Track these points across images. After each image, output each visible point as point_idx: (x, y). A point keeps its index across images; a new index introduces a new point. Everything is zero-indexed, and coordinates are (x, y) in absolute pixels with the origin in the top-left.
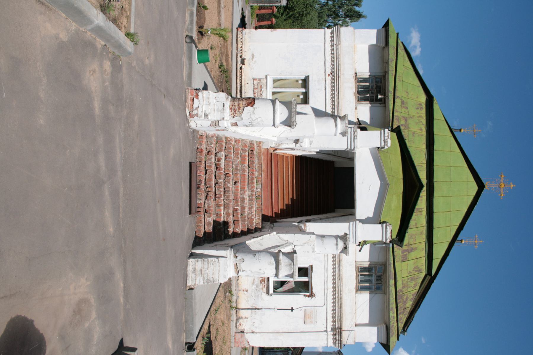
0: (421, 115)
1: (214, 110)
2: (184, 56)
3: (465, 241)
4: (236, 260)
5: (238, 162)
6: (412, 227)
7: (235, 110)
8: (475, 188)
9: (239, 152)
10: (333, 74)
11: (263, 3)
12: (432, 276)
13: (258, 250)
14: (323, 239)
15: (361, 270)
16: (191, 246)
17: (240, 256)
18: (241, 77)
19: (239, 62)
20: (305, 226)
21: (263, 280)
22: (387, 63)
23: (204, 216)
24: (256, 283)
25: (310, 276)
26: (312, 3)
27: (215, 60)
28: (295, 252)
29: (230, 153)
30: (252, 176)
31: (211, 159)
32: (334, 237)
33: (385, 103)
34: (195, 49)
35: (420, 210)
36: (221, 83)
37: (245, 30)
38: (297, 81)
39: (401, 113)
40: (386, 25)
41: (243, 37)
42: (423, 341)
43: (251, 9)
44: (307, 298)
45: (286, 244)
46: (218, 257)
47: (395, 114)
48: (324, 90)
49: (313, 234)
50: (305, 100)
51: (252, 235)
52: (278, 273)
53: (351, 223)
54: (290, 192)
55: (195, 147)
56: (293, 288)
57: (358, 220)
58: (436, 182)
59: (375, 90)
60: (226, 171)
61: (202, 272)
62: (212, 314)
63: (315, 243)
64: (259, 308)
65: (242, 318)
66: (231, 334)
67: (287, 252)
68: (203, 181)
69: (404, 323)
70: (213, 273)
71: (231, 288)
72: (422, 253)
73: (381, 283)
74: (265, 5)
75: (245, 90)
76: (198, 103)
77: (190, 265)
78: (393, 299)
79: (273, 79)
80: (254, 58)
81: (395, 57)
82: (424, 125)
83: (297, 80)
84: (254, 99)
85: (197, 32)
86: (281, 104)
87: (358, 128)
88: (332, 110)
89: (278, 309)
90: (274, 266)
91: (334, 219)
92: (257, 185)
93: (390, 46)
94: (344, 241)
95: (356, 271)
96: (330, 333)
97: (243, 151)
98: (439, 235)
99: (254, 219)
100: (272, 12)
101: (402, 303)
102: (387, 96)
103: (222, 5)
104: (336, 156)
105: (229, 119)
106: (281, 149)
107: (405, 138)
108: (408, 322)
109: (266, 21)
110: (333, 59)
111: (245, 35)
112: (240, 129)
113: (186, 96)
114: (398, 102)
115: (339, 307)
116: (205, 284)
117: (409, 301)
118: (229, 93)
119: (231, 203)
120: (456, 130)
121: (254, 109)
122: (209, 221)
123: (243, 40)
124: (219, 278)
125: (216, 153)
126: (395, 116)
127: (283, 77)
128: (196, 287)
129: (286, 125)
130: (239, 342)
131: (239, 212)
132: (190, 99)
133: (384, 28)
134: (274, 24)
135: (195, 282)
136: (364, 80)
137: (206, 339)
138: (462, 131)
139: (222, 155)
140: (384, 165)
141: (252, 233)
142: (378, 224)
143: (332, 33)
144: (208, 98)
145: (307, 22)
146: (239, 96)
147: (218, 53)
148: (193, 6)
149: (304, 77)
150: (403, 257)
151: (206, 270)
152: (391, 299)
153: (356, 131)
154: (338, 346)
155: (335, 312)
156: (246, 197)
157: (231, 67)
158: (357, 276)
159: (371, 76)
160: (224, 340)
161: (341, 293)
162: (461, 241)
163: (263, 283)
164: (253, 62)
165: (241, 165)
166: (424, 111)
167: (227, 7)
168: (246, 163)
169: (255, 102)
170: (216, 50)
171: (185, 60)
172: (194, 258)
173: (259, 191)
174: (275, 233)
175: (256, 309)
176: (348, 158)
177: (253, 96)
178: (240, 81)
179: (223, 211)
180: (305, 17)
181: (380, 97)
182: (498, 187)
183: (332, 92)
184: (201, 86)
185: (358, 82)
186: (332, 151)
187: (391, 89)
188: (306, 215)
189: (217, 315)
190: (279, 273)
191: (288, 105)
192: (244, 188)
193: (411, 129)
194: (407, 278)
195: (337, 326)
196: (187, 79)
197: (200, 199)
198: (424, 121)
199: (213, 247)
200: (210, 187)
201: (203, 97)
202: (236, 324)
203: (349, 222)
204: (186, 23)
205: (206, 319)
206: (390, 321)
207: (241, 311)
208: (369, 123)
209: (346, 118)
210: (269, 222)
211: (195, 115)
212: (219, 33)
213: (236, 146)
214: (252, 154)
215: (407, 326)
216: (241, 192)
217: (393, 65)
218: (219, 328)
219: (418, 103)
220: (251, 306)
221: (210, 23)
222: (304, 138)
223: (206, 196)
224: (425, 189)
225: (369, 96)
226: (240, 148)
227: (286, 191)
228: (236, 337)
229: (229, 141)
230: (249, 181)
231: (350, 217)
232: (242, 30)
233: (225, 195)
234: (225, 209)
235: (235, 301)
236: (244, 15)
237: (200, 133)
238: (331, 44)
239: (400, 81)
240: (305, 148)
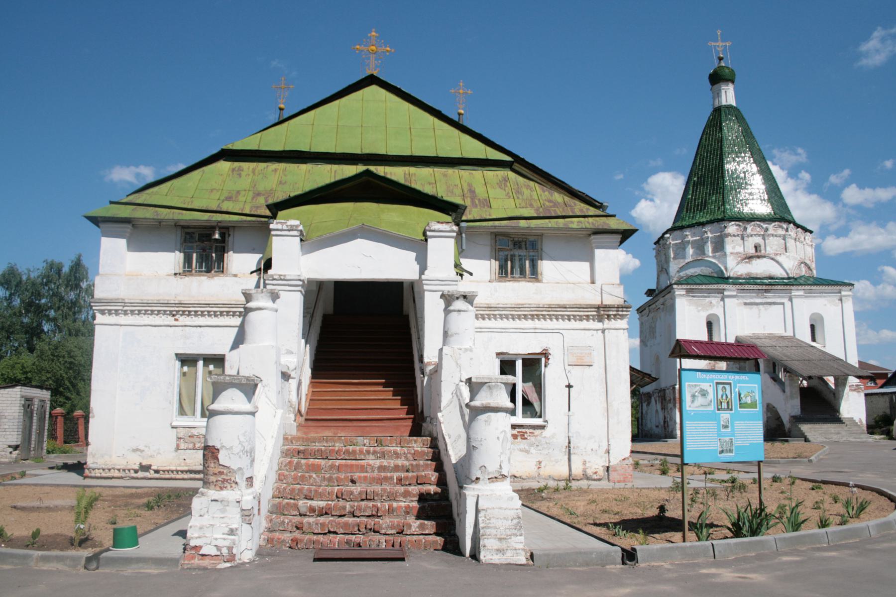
0: (251, 169)
1: (223, 518)
2: (122, 573)
3: (460, 109)
4: (483, 480)
5: (317, 476)
6: (435, 190)
7: (224, 481)
8: (373, 90)
9: (299, 474)
10: (174, 313)
11: (44, 432)
12: (512, 160)
13: (466, 442)
14: (449, 333)
15: (503, 273)
16: (460, 557)
17: (476, 473)
18: (172, 471)
19: (147, 474)
20: (429, 364)
21: (521, 435)
22: (160, 223)
23: (408, 536)
24: (527, 448)
25: (515, 357)
26: (51, 347)
27: (137, 516)
28: (469, 381)
29: (300, 490)
30: (342, 453)
31: (309, 523)
32: (446, 315)
33: (227, 228)
34: (111, 552)
35: (407, 176)
36: (179, 506)
37: (88, 463)
38: (184, 374)
39: (245, 202)
40: (96, 220)
41: (101, 467)
42: (621, 177)
43: (53, 453)
44: (550, 362)
45: (457, 396)
46: (477, 511)
47: (247, 211)
48: (202, 328)
49: (441, 350)
50: (218, 360)
51: (442, 453)
52: (503, 408)
53: (425, 287)
54: (373, 389)
55: (288, 551)
56: (535, 386)
57: (420, 277)
58: (362, 149)
59: (206, 243)
60: (332, 497)
61: (503, 539)
62: (576, 521)
63: (456, 347)
64: (567, 441)
65: (584, 471)
66: (611, 487)
67: (469, 394)
68: (347, 537)
69: (588, 207)
70: (504, 518)
71: (534, 489)
72: (477, 175)
73: (525, 241)
74: (46, 428)
75: (195, 465)
76: (209, 546)
77: (491, 559)
78: (550, 222)
79: (179, 415)
80: (139, 448)
81: (152, 208)
82: (267, 166)
83: (182, 374)
84: (206, 448)
85: (80, 548)
86: (216, 401)
87: (267, 273)
88: (237, 315)
89: (569, 410)
90: (492, 415)
91: (419, 315)
92: (358, 444)
93: (132, 216)
94: (454, 300)
95: (505, 282)
96: (607, 324)
97: (298, 469)
98: (449, 149)
99: (416, 449)
100: (61, 416)
101: (557, 209)
102: (216, 224)
103: (36, 504)
104: (314, 311)
105: (239, 492)
106: (299, 404)
107: (288, 197)
108: (587, 200)
109: (78, 428)
110: (148, 313)
111: (97, 463)
112: (259, 472)
113: (195, 569)
114: (227, 206)
115: (565, 309)
116: (523, 532)
117: (553, 198)
118: (195, 491)
119: (387, 489)
120: (281, 115)
121: (224, 448)
122: (418, 527)
123: (106, 467)
124: (512, 509)
125: (300, 515)
126: (251, 211)
127: (176, 398)
128: (528, 549)
129: (254, 394)
130: (623, 474)
131: (403, 475)
132: (201, 561)
133: (100, 225)
134: (84, 414)
135: (519, 549)
136: (188, 261)
137: (617, 530)
138: (282, 106)
139: (303, 504)
140: (331, 231)
141: (439, 452)
142: (427, 244)
143: (102, 312)
144: (201, 528)
145: (84, 356)
146: (201, 476)
147: (124, 511)
148: (30, 556)
149: (177, 361)
150: (482, 205)
151: (499, 531)
152: (550, 225)
153: (272, 276)
154: (627, 311)
155: (573, 315)
156: (378, 463)
157: (153, 489)
158: (514, 279)
159: (182, 250)
160: (621, 501)
161: (541, 306)
162: (460, 114)
163: (525, 434)
164: (146, 449)
165: (323, 472)
166: (245, 165)
167: (41, 496)
168: (319, 463)
169: (211, 445)
170: (119, 515)
171: (129, 571)
172: (479, 552)
173: (368, 441)
174: (439, 415)
175: (569, 447)
176: (319, 291)
177: (201, 452)
178: (179, 472)
179: (400, 503)
180: (74, 359)
181: (217, 236)
182: (374, 56)
183: (205, 315)
184: (180, 541)
185: (191, 271)
186: (304, 317)
187: (206, 216)
188: (412, 362)
189: (579, 512)
190: (504, 406)
191: (218, 389)
192: (362, 466)
193: (274, 186)
194: (517, 200)
195: (595, 313)
196: (165, 567)
197: (379, 542)
198: (262, 165)
199: (460, 520)
200: (359, 526)
201: (199, 537)
202: (595, 480)
203: (424, 291)
204: (60, 568)
205: (584, 530)
206: (585, 228)
207: (574, 471)
208: (261, 255)
209: (248, 292)
210: (422, 426)
211: (230, 553)
212: (85, 508)
213: (290, 480)
214: (303, 452)
215: (594, 202)
216: (369, 470)
217: (165, 213)
218: (601, 509)
219: (231, 174)
220: (565, 454)
221: (65, 525)
222: (280, 364)
223: (375, 532)
224: (372, 168)
225: (216, 255)
226: (293, 474)
227: (372, 395)
228: (616, 480)
229: (279, 492)
230: (351, 458)
231: (416, 290)
232: (88, 469)
233: (374, 499)
234: (397, 499)
235: (556, 483)
236: (62, 466)
237: (263, 543)
238: (123, 315)
239: (192, 202)
240: (298, 362)
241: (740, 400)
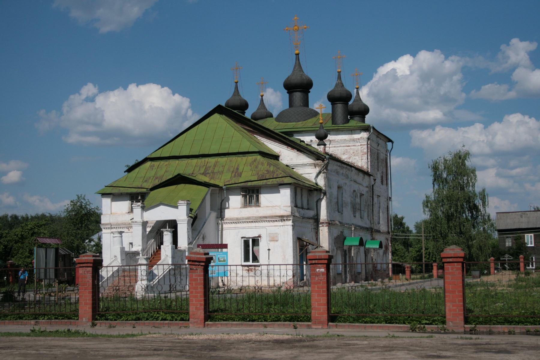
203: (177, 224)
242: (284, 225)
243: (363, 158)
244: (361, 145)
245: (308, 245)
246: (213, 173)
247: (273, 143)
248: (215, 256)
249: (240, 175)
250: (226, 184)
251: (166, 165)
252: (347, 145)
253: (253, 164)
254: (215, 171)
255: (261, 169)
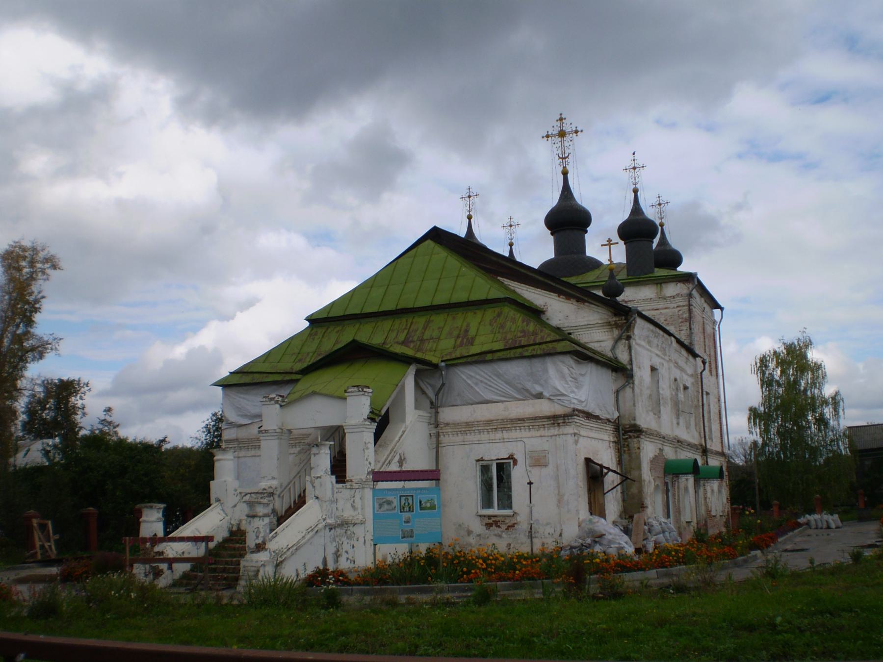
89: (531, 502)
241: (420, 505)
242: (559, 435)
243: (682, 328)
244: (677, 307)
245: (606, 474)
246: (422, 341)
247: (532, 289)
248: (412, 496)
249: (471, 342)
250: (444, 359)
251: (338, 331)
252: (655, 307)
253: (495, 322)
254: (425, 337)
255: (511, 328)
